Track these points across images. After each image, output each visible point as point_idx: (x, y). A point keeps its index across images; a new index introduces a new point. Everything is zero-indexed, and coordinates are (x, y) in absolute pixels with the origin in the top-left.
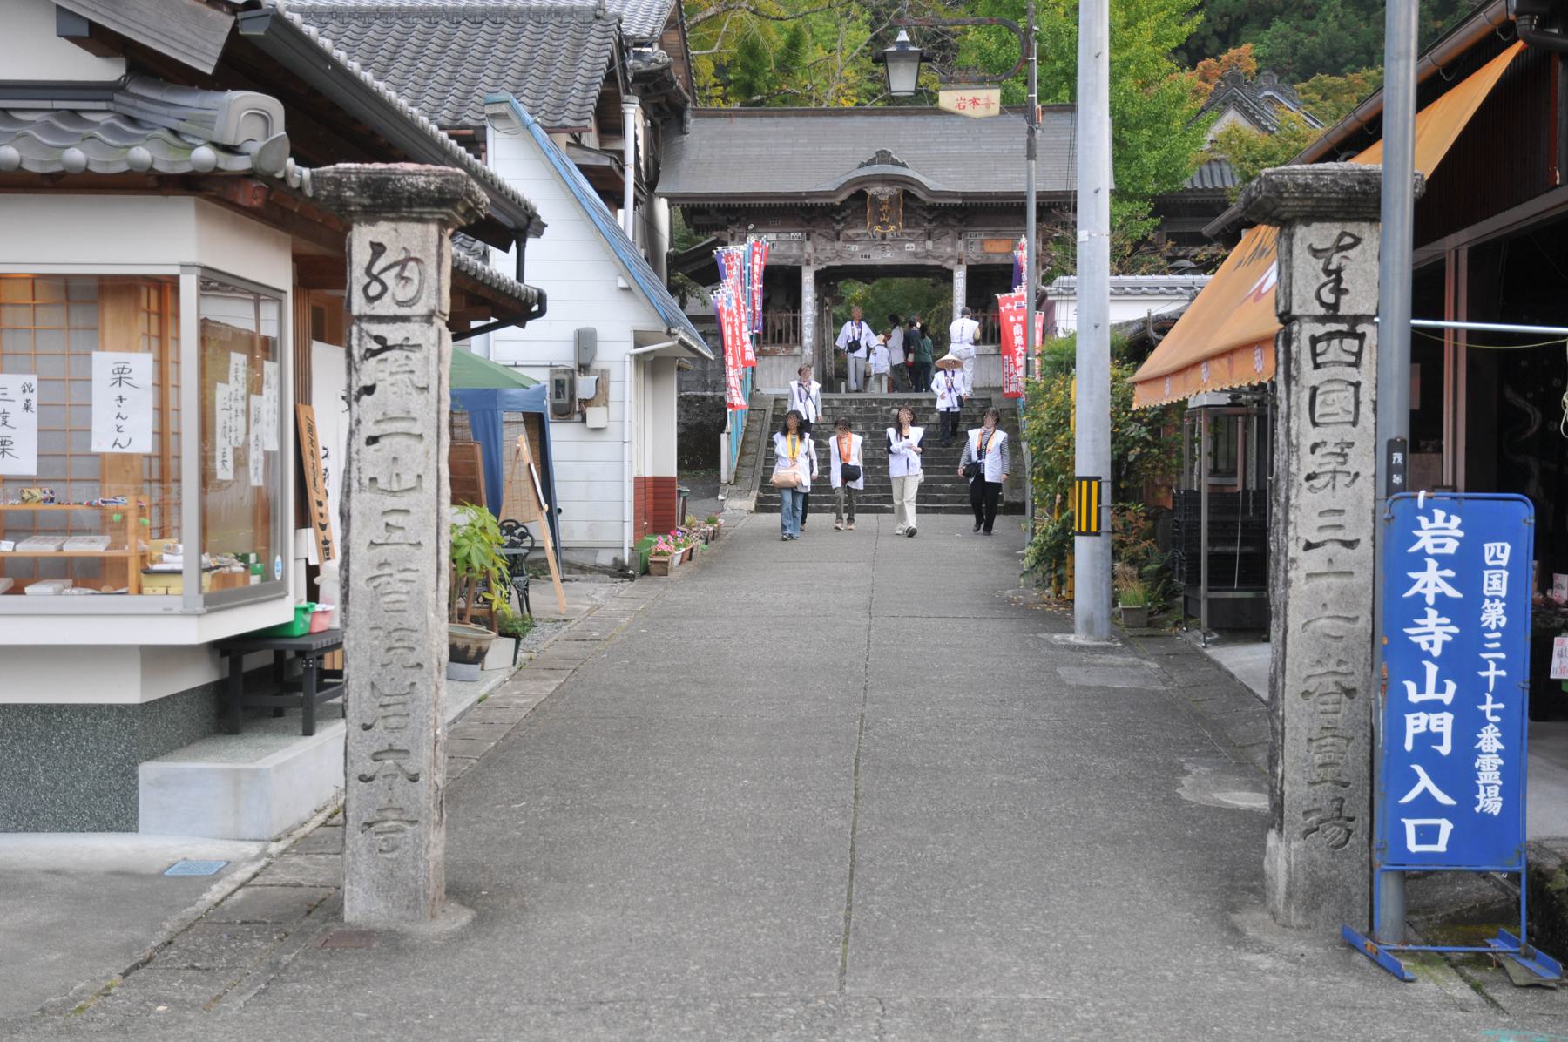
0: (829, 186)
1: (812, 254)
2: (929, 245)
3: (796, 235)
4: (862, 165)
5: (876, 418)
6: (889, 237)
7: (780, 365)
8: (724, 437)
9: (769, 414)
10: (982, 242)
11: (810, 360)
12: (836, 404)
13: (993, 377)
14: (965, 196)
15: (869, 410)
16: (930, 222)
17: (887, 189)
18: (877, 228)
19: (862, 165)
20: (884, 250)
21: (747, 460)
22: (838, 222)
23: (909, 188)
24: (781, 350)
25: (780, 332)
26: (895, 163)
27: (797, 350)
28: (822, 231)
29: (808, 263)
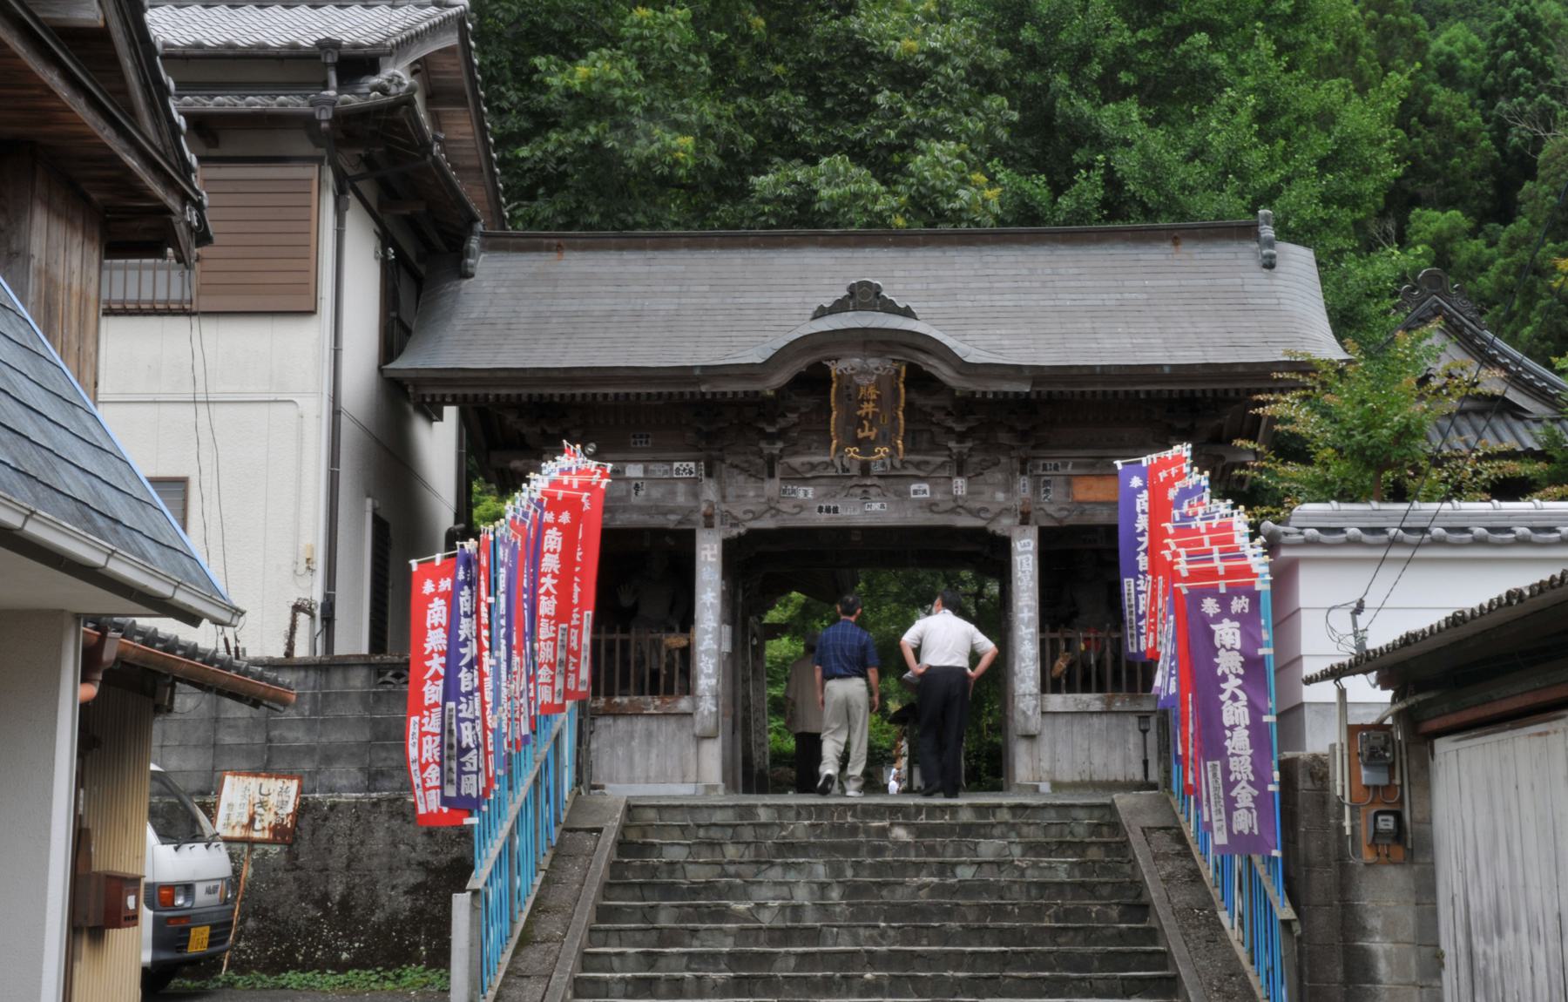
0: (755, 356)
1: (722, 512)
2: (960, 486)
3: (685, 467)
4: (821, 313)
5: (854, 849)
6: (877, 469)
7: (649, 734)
8: (461, 903)
9: (609, 838)
10: (1069, 480)
11: (710, 723)
12: (764, 816)
13: (1098, 760)
14: (1039, 374)
15: (838, 829)
16: (961, 437)
17: (873, 363)
18: (852, 452)
19: (821, 313)
20: (866, 497)
21: (533, 955)
22: (771, 438)
23: (922, 359)
24: (653, 703)
25: (655, 675)
26: (890, 308)
27: (684, 704)
28: (737, 460)
29: (709, 525)
